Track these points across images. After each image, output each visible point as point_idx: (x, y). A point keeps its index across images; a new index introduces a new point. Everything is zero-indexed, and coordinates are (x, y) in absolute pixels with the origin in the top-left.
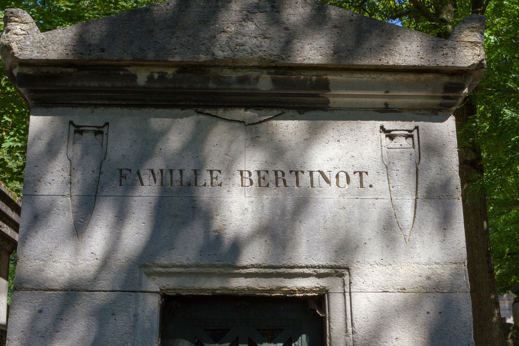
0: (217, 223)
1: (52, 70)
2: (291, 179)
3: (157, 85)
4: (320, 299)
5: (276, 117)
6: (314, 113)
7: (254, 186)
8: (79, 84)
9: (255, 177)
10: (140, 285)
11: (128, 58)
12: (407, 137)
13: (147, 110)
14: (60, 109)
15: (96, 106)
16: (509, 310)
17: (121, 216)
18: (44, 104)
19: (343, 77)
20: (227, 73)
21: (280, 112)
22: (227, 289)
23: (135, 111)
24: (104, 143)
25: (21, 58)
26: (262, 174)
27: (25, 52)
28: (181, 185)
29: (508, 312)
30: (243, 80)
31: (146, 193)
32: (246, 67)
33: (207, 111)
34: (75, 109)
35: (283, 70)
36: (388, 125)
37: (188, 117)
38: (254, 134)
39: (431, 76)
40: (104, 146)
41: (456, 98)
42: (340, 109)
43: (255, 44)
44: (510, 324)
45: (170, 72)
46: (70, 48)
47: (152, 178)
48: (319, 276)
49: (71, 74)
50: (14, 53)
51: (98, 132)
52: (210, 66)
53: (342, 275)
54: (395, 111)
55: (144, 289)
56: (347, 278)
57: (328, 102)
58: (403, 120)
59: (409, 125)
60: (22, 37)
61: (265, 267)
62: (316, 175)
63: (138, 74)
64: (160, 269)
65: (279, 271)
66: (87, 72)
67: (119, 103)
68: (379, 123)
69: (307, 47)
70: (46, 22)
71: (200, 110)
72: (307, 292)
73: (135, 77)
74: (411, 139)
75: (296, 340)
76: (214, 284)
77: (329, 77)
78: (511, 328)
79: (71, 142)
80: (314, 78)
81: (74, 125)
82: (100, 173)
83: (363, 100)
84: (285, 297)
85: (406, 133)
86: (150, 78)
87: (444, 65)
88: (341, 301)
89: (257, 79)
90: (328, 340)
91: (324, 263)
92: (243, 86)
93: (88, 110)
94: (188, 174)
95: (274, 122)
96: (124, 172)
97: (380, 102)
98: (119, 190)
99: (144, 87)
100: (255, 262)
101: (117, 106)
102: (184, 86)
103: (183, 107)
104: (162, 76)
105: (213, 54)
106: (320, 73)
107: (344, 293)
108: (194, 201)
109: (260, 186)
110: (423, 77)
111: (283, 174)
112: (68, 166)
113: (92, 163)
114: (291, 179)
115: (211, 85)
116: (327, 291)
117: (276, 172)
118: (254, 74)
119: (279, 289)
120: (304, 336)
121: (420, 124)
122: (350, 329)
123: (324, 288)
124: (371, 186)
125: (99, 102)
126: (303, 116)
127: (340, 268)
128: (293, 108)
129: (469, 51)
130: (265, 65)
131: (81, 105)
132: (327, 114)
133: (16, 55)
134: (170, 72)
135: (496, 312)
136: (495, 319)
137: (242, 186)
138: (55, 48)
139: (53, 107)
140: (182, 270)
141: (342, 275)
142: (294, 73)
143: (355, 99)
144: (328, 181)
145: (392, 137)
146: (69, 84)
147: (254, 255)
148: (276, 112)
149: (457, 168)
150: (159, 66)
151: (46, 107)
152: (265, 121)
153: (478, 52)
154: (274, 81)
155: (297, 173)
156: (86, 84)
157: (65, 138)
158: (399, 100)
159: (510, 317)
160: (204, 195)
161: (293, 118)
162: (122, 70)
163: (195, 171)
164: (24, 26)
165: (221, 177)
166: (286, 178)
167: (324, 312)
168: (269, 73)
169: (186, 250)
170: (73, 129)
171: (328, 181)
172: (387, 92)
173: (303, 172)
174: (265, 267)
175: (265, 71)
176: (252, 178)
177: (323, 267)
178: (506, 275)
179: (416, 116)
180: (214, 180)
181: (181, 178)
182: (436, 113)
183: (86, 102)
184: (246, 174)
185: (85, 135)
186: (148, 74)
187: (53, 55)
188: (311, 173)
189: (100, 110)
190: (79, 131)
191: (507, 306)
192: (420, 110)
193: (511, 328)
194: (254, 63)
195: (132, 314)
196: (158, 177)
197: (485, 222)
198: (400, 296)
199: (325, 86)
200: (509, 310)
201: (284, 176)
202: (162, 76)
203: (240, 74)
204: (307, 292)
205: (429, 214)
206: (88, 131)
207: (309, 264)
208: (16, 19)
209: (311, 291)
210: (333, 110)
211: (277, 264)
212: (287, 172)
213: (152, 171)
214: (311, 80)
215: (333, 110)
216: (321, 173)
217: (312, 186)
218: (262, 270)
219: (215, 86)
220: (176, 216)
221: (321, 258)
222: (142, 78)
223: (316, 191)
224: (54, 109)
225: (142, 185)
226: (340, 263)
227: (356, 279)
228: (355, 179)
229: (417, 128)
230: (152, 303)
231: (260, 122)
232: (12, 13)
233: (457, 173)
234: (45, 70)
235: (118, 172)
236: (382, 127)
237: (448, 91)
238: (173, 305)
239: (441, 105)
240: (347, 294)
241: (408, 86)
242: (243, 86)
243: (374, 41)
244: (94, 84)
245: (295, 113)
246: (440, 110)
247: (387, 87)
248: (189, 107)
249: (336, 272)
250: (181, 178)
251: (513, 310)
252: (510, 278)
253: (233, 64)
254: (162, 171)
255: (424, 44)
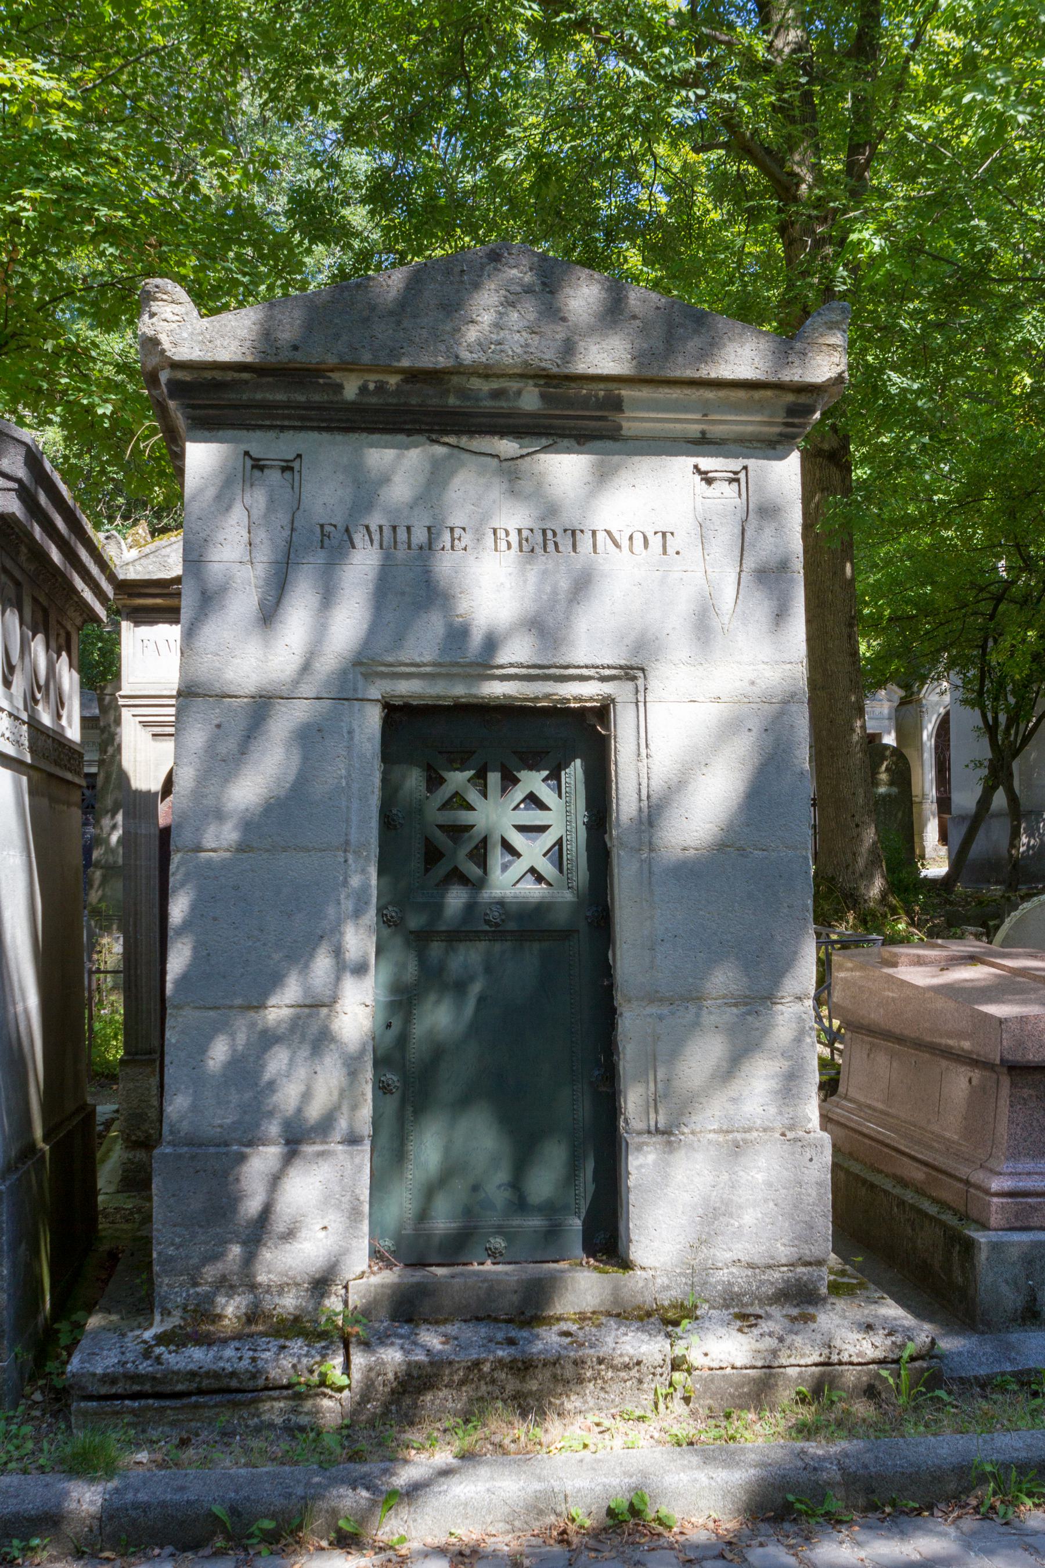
0: (463, 606)
1: (218, 375)
2: (565, 543)
3: (374, 400)
4: (603, 712)
5: (545, 449)
6: (598, 444)
7: (512, 551)
8: (259, 396)
9: (514, 538)
10: (355, 690)
11: (332, 360)
12: (731, 481)
13: (357, 435)
14: (230, 433)
15: (282, 428)
16: (890, 719)
17: (328, 597)
18: (209, 424)
19: (644, 393)
20: (476, 384)
21: (551, 442)
22: (475, 696)
23: (339, 437)
24: (296, 484)
25: (176, 358)
26: (525, 533)
27: (181, 349)
28: (409, 548)
29: (886, 722)
30: (497, 394)
31: (363, 564)
32: (503, 376)
33: (446, 439)
34: (251, 434)
35: (557, 383)
36: (706, 463)
37: (416, 447)
38: (512, 475)
39: (769, 393)
40: (297, 490)
41: (802, 426)
42: (636, 438)
43: (517, 342)
44: (887, 747)
45: (393, 380)
46: (248, 343)
47: (367, 537)
48: (603, 679)
49: (246, 382)
50: (163, 351)
51: (287, 468)
52: (452, 373)
53: (634, 678)
54: (716, 443)
55: (360, 696)
56: (640, 682)
57: (620, 428)
58: (726, 457)
59: (735, 464)
60: (175, 325)
61: (528, 667)
62: (601, 536)
63: (345, 383)
64: (383, 669)
65: (547, 671)
66: (270, 379)
67: (315, 424)
68: (692, 460)
69: (594, 349)
70: (207, 299)
71: (434, 437)
72: (586, 701)
73: (340, 387)
74: (736, 484)
75: (567, 766)
76: (459, 691)
77: (623, 392)
78: (888, 753)
79: (248, 484)
80: (602, 393)
81: (251, 457)
82: (292, 530)
83: (672, 426)
84: (555, 707)
85: (731, 475)
86: (363, 390)
87: (788, 379)
88: (633, 713)
89: (519, 393)
90: (613, 767)
91: (610, 662)
92: (497, 404)
93: (271, 435)
94: (420, 536)
95: (542, 457)
96: (328, 529)
97: (694, 429)
98: (320, 557)
99: (353, 403)
100: (514, 659)
101: (312, 429)
102: (413, 402)
103: (409, 433)
104: (381, 387)
105: (457, 357)
106: (611, 386)
107: (637, 703)
108: (428, 572)
109: (521, 551)
110: (758, 394)
111: (555, 534)
112: (246, 519)
113: (282, 518)
114: (565, 543)
115: (452, 401)
116: (613, 701)
117: (544, 531)
118: (514, 385)
119: (547, 697)
120: (578, 761)
121: (751, 463)
122: (643, 751)
123: (610, 696)
124: (678, 553)
125: (286, 423)
126: (583, 448)
127: (632, 668)
128: (569, 436)
129: (826, 364)
130: (532, 372)
131: (260, 427)
132: (617, 445)
133: (168, 354)
134: (393, 380)
135: (859, 723)
136: (855, 738)
137: (496, 550)
138: (225, 344)
139: (218, 429)
140: (413, 669)
141: (634, 678)
142: (573, 385)
143: (658, 425)
144: (617, 545)
145: (709, 481)
146: (245, 397)
147: (517, 652)
148: (544, 442)
149: (799, 529)
150: (377, 372)
151: (209, 429)
152: (528, 454)
153: (836, 360)
154: (543, 396)
155: (573, 532)
156: (269, 396)
157: (240, 475)
158: (721, 427)
159: (889, 733)
160: (445, 564)
161: (569, 451)
162: (323, 377)
163: (429, 528)
164: (177, 309)
165: (467, 539)
166: (558, 539)
167: (607, 728)
168: (536, 385)
169: (423, 645)
170: (249, 463)
171: (617, 545)
172: (705, 415)
173: (582, 531)
174: (528, 667)
175: (531, 382)
176: (510, 538)
177: (609, 667)
178: (882, 658)
179: (745, 450)
180: (456, 542)
181: (409, 538)
182: (772, 446)
183: (268, 423)
184: (503, 534)
185: (266, 471)
186: (360, 383)
187: (225, 355)
188: (594, 533)
189: (289, 435)
190: (258, 466)
191: (886, 711)
192: (750, 441)
193: (888, 753)
194: (516, 371)
195: (345, 730)
196: (376, 537)
197: (848, 565)
198: (715, 709)
199: (617, 404)
200: (890, 719)
201: (552, 536)
202: (381, 387)
203: (495, 385)
204: (586, 701)
205: (760, 608)
206: (271, 467)
207: (589, 662)
208: (165, 297)
209: (591, 699)
210: (627, 439)
211: (545, 662)
212: (559, 532)
213: (367, 528)
214: (596, 396)
215: (627, 439)
216: (608, 533)
217: (595, 552)
218: (524, 671)
219: (458, 403)
220: (403, 594)
221: (610, 656)
222: (351, 390)
223: (600, 558)
224: (221, 433)
225: (354, 547)
226: (633, 662)
227: (653, 683)
228: (656, 542)
229: (745, 468)
230: (373, 718)
231: (522, 456)
232: (157, 287)
233: (799, 536)
234: (208, 375)
235: (318, 529)
236: (696, 467)
237: (789, 415)
238: (399, 716)
239: (781, 434)
240: (641, 705)
241: (736, 407)
242: (497, 404)
243: (693, 345)
244: (281, 397)
245: (572, 443)
246: (779, 442)
247: (706, 408)
248: (419, 432)
249: (627, 674)
250: (409, 538)
251: (897, 720)
252: (888, 663)
253: (486, 373)
254: (381, 527)
255: (762, 347)
